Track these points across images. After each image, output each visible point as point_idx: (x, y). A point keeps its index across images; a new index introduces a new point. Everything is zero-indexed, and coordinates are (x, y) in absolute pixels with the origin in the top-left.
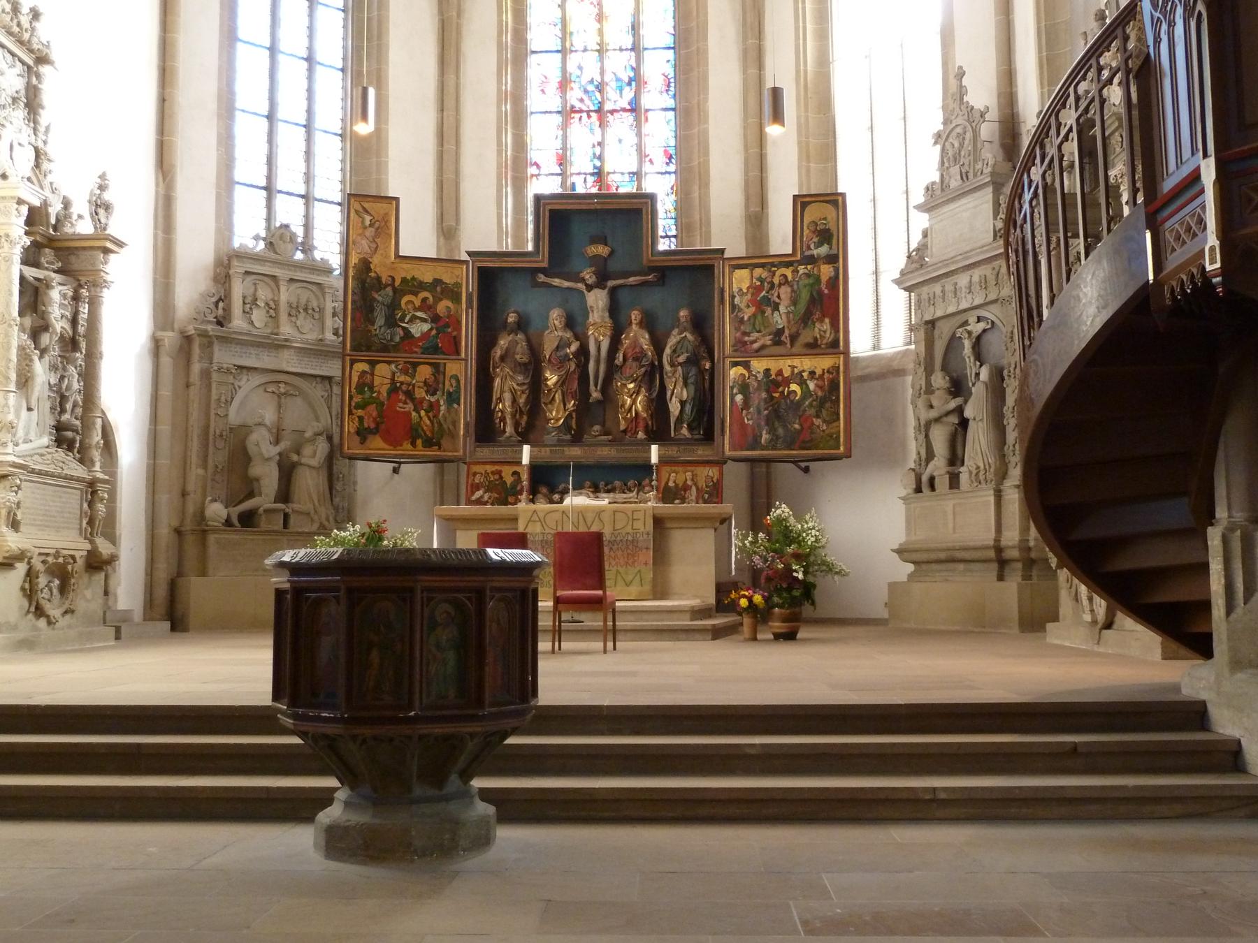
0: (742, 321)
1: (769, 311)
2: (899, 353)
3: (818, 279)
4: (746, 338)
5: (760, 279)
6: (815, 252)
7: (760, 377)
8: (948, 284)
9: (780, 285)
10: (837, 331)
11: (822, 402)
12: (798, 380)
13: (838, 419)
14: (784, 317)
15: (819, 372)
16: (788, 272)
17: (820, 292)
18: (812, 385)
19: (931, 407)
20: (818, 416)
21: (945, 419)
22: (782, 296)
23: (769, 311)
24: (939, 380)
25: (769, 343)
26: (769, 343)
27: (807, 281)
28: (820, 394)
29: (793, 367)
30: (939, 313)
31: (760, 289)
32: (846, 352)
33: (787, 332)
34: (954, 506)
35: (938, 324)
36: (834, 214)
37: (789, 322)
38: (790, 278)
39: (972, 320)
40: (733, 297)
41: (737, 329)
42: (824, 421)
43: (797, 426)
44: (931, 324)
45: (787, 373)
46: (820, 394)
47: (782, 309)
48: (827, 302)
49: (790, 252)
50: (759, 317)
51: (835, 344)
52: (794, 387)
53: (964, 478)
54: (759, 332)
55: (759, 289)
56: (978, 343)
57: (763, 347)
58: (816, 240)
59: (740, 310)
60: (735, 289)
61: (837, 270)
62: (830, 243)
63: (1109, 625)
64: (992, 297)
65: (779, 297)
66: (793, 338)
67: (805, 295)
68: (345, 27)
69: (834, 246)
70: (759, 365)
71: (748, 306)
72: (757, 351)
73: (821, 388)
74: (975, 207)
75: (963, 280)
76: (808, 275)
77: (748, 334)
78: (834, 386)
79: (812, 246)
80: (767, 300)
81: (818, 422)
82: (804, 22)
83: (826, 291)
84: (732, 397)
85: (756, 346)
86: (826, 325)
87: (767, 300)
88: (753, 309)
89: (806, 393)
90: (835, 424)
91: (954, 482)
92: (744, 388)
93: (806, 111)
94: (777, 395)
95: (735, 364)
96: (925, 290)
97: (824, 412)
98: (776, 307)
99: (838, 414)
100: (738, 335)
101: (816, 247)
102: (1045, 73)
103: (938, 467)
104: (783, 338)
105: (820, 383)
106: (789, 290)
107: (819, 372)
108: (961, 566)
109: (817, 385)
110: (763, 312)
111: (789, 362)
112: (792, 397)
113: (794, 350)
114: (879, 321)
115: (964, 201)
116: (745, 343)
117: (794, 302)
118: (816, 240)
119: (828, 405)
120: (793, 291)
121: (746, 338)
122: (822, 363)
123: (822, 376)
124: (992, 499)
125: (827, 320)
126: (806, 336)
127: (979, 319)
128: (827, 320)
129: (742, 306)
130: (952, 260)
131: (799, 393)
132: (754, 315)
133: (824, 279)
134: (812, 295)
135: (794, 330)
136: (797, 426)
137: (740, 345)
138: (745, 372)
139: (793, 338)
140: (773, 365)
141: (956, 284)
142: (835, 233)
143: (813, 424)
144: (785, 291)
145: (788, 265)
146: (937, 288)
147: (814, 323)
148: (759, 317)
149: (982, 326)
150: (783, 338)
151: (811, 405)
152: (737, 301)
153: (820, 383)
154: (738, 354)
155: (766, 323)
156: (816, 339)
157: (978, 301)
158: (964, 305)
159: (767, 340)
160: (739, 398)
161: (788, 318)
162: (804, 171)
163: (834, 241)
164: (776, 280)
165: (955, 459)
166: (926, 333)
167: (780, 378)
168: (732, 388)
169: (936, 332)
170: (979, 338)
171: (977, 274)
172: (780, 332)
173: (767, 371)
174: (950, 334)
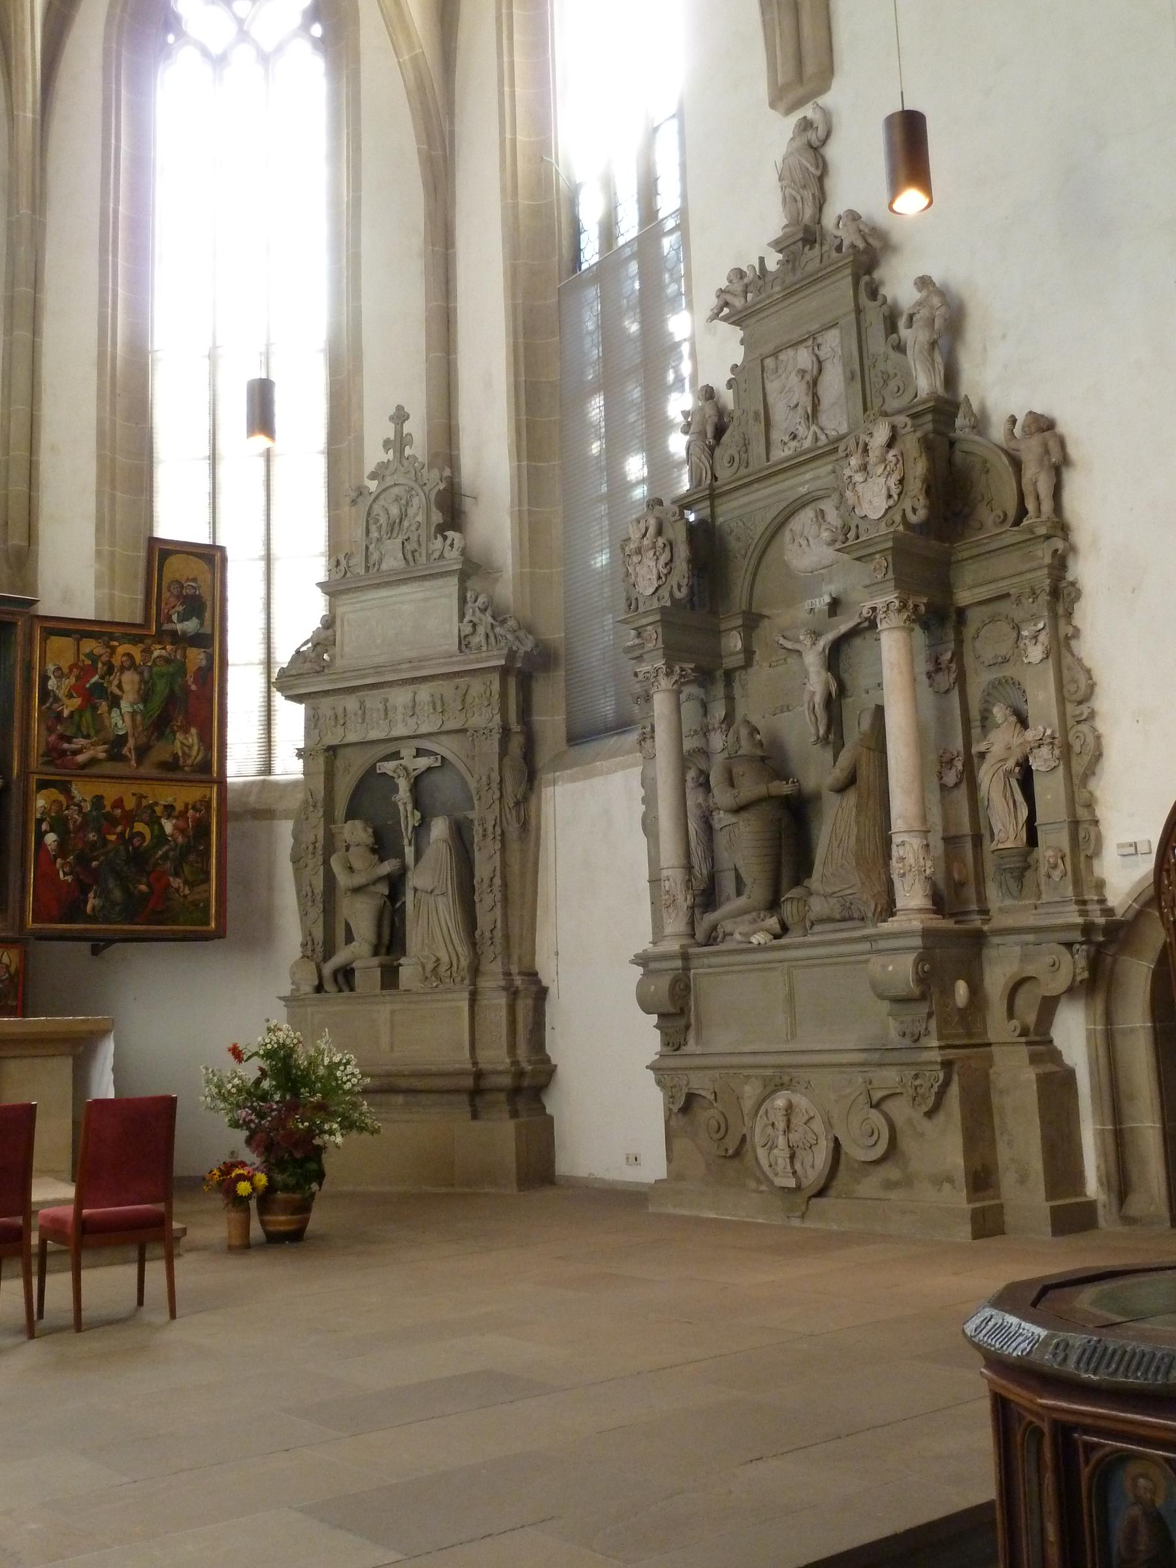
0: (59, 716)
1: (104, 706)
2: (253, 783)
3: (182, 669)
4: (66, 746)
5: (90, 655)
6: (179, 627)
7: (87, 807)
8: (373, 701)
9: (122, 669)
10: (209, 748)
11: (184, 853)
12: (146, 816)
13: (207, 880)
14: (127, 718)
15: (179, 807)
16: (136, 652)
17: (186, 689)
18: (168, 826)
19: (351, 869)
20: (177, 874)
21: (372, 888)
22: (126, 687)
23: (104, 706)
24: (356, 833)
25: (102, 755)
26: (102, 755)
27: (164, 669)
28: (180, 839)
29: (142, 797)
30: (352, 738)
31: (93, 669)
32: (221, 781)
33: (131, 742)
34: (393, 1012)
35: (341, 753)
36: (209, 576)
37: (134, 726)
38: (138, 658)
39: (407, 752)
40: (44, 679)
41: (51, 730)
42: (186, 882)
43: (143, 887)
44: (332, 751)
45: (130, 804)
46: (180, 839)
47: (125, 706)
48: (189, 701)
49: (139, 620)
50: (88, 716)
51: (205, 767)
52: (139, 827)
53: (408, 972)
54: (88, 737)
55: (85, 672)
56: (416, 784)
57: (93, 761)
58: (180, 608)
59: (57, 699)
60: (51, 668)
61: (210, 658)
62: (200, 617)
63: (233, 1153)
64: (451, 725)
65: (120, 686)
66: (142, 752)
67: (161, 688)
68: (556, 144)
69: (207, 623)
70: (82, 791)
71: (70, 696)
72: (84, 766)
73: (183, 831)
74: (426, 600)
75: (400, 697)
76: (167, 661)
77: (69, 740)
78: (202, 830)
79: (175, 618)
80: (100, 690)
81: (176, 882)
82: (115, 284)
83: (193, 687)
84: (40, 836)
85: (81, 758)
86: (193, 738)
87: (100, 690)
88: (77, 702)
89: (161, 838)
90: (204, 887)
91: (390, 978)
92: (59, 824)
93: (113, 412)
94: (113, 838)
95: (43, 785)
96: (326, 704)
97: (186, 868)
98: (115, 702)
99: (208, 873)
100: (52, 738)
101: (181, 620)
102: (524, 443)
103: (358, 951)
104: (125, 751)
105: (181, 823)
106: (136, 678)
107: (179, 807)
108: (400, 1099)
109: (176, 827)
110: (95, 708)
111: (135, 788)
112: (136, 842)
113: (143, 771)
114: (262, 738)
115: (404, 589)
116: (63, 753)
117: (145, 696)
118: (180, 608)
119: (192, 857)
120: (142, 681)
121: (66, 746)
122: (183, 795)
123: (183, 815)
124: (465, 1005)
125: (193, 731)
126: (162, 752)
127: (420, 753)
128: (193, 731)
129: (61, 694)
130: (394, 666)
131: (148, 837)
132: (80, 710)
133: (191, 668)
134: (172, 691)
135: (143, 740)
136: (143, 887)
137: (54, 755)
138: (62, 798)
139: (142, 752)
140: (110, 792)
141: (386, 700)
142: (209, 604)
143: (169, 885)
144: (130, 680)
145: (136, 640)
146: (351, 703)
147: (174, 733)
148: (88, 716)
149: (423, 763)
150: (125, 751)
151: (165, 857)
152: (52, 684)
153: (181, 823)
154: (52, 769)
155: (99, 724)
156: (176, 756)
157: (424, 729)
158: (400, 731)
159: (100, 752)
160: (51, 839)
161: (133, 719)
162: (106, 501)
163: (207, 615)
164: (117, 661)
165: (391, 941)
166: (326, 763)
167: (118, 812)
168: (39, 822)
169: (340, 763)
170: (417, 778)
171: (424, 693)
172: (121, 740)
173: (98, 800)
174: (367, 766)
